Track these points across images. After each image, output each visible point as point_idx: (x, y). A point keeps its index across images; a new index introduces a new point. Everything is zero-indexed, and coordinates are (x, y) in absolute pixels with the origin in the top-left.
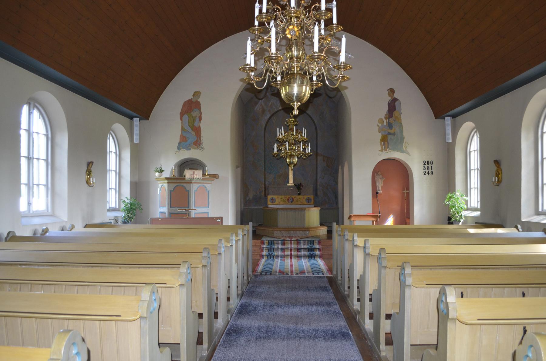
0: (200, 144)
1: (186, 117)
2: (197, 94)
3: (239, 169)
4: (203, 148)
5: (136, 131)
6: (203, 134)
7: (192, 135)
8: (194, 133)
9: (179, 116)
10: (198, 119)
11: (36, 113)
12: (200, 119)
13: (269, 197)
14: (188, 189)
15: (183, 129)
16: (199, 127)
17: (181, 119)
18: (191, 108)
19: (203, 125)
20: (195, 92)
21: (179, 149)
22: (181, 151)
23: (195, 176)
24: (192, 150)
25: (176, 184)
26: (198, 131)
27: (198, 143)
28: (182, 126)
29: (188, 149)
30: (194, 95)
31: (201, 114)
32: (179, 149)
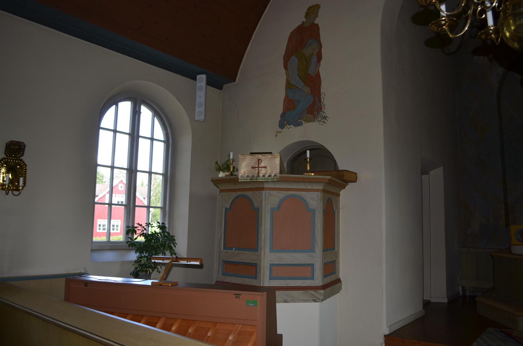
0: (320, 109)
1: (294, 60)
2: (313, 11)
3: (437, 175)
4: (325, 118)
5: (201, 97)
6: (325, 88)
8: (307, 89)
9: (282, 61)
10: (315, 59)
11: (146, 113)
12: (319, 57)
13: (106, 231)
14: (256, 205)
15: (289, 86)
16: (318, 75)
17: (286, 67)
18: (305, 41)
19: (326, 71)
20: (310, 8)
21: (282, 125)
22: (285, 130)
23: (263, 171)
24: (306, 125)
25: (235, 195)
26: (314, 83)
27: (314, 110)
28: (287, 80)
29: (297, 124)
30: (307, 15)
31: (321, 46)
32: (282, 125)
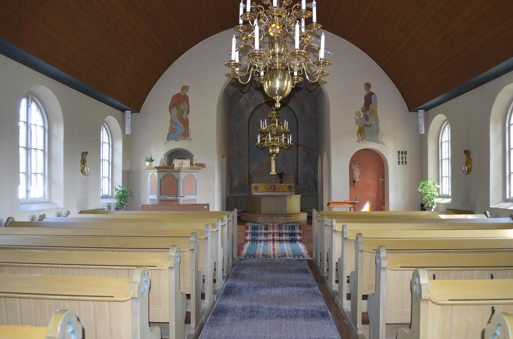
0: (188, 135)
1: (175, 110)
2: (185, 88)
3: (225, 158)
4: (191, 139)
5: (128, 123)
6: (191, 126)
7: (180, 127)
8: (182, 125)
9: (168, 109)
10: (186, 112)
11: (33, 106)
12: (188, 112)
13: (253, 185)
14: (176, 178)
15: (172, 121)
16: (187, 119)
17: (170, 112)
18: (180, 101)
19: (191, 118)
20: (183, 87)
21: (168, 139)
22: (170, 142)
23: (184, 166)
24: (181, 141)
25: (166, 173)
26: (186, 123)
27: (186, 135)
28: (171, 119)
29: (176, 140)
30: (182, 89)
31: (189, 107)
32: (168, 139)
